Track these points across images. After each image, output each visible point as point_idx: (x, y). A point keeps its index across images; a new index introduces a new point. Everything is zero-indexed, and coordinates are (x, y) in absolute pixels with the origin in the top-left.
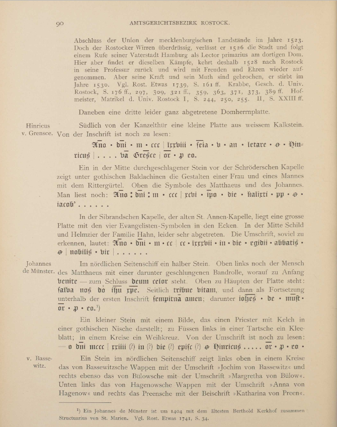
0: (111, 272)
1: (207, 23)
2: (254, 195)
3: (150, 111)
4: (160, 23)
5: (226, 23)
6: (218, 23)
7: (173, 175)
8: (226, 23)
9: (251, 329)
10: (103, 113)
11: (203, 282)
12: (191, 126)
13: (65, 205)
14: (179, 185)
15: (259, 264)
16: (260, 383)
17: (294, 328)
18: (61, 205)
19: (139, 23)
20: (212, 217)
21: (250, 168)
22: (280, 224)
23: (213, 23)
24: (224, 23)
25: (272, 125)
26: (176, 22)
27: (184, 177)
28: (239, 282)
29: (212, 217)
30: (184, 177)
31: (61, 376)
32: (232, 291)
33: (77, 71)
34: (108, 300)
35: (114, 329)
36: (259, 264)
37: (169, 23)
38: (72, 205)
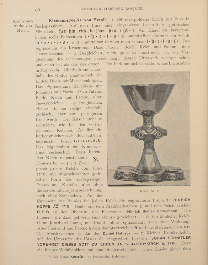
1: (129, 9)
3: (92, 52)
4: (100, 9)
5: (141, 9)
6: (136, 9)
8: (141, 9)
11: (75, 212)
12: (38, 109)
15: (61, 76)
17: (149, 233)
20: (81, 130)
22: (86, 211)
23: (133, 9)
24: (140, 8)
26: (110, 9)
27: (37, 104)
29: (81, 130)
30: (140, 58)
31: (46, 65)
32: (145, 228)
33: (100, 19)
34: (92, 64)
35: (56, 76)
36: (61, 76)
37: (106, 9)
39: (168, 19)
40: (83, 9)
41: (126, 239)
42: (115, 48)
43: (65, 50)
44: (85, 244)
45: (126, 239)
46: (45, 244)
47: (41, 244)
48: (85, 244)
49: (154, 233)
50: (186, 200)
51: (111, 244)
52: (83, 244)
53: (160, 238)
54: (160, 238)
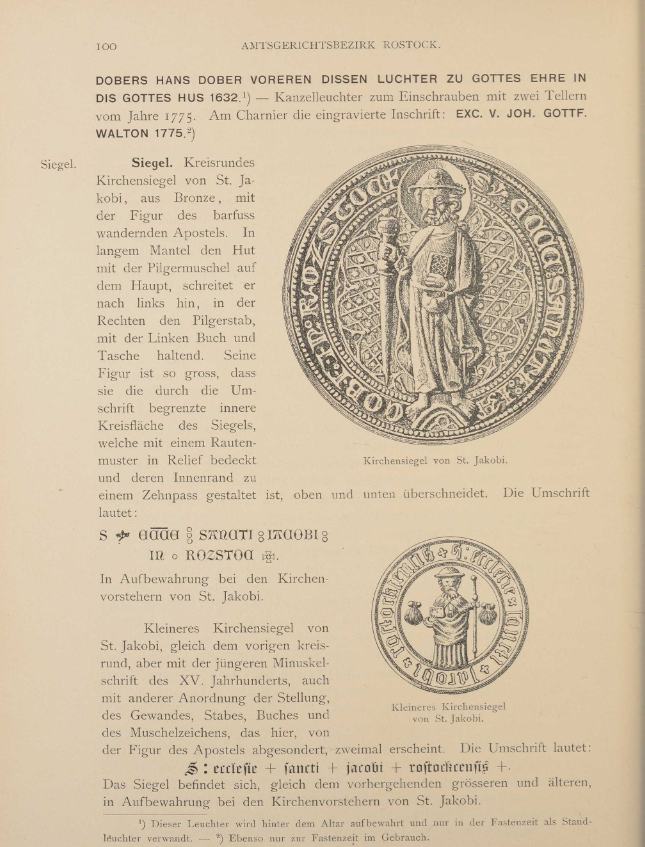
0: (177, 661)
2: (552, 77)
5: (432, 45)
6: (417, 45)
7: (209, 388)
8: (432, 45)
9: (105, 356)
10: (556, 782)
13: (363, 769)
14: (467, 799)
16: (129, 678)
18: (101, 134)
19: (260, 46)
21: (468, 784)
23: (406, 45)
24: (429, 44)
25: (528, 492)
27: (385, 838)
28: (160, 287)
30: (135, 717)
38: (185, 839)
39: (371, 839)
40: (249, 46)
41: (374, 116)
42: (139, 182)
43: (228, 121)
44: (491, 78)
45: (374, 116)
46: (294, 80)
47: (262, 80)
48: (491, 78)
49: (180, 444)
50: (399, 79)
51: (358, 78)
52: (485, 78)
53: (165, 81)
54: (165, 81)
